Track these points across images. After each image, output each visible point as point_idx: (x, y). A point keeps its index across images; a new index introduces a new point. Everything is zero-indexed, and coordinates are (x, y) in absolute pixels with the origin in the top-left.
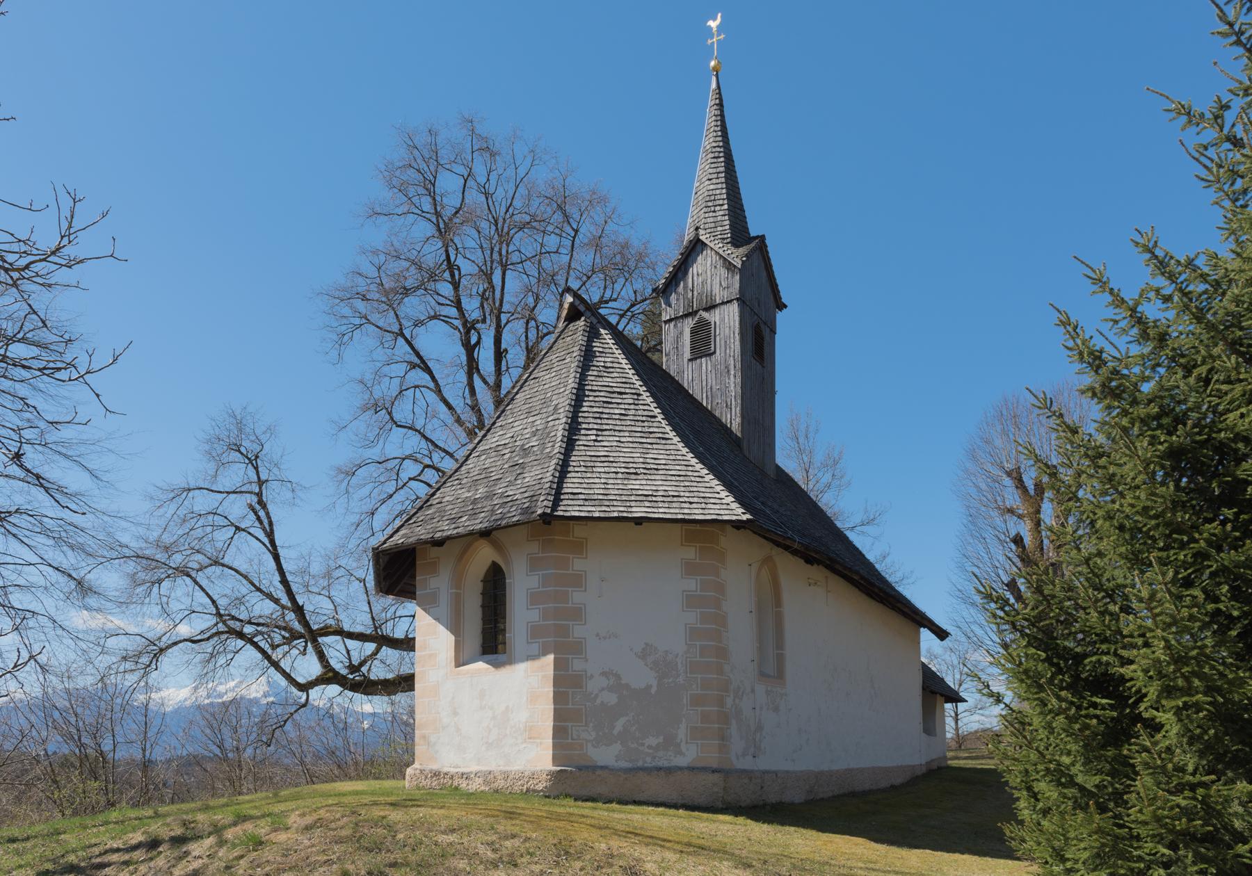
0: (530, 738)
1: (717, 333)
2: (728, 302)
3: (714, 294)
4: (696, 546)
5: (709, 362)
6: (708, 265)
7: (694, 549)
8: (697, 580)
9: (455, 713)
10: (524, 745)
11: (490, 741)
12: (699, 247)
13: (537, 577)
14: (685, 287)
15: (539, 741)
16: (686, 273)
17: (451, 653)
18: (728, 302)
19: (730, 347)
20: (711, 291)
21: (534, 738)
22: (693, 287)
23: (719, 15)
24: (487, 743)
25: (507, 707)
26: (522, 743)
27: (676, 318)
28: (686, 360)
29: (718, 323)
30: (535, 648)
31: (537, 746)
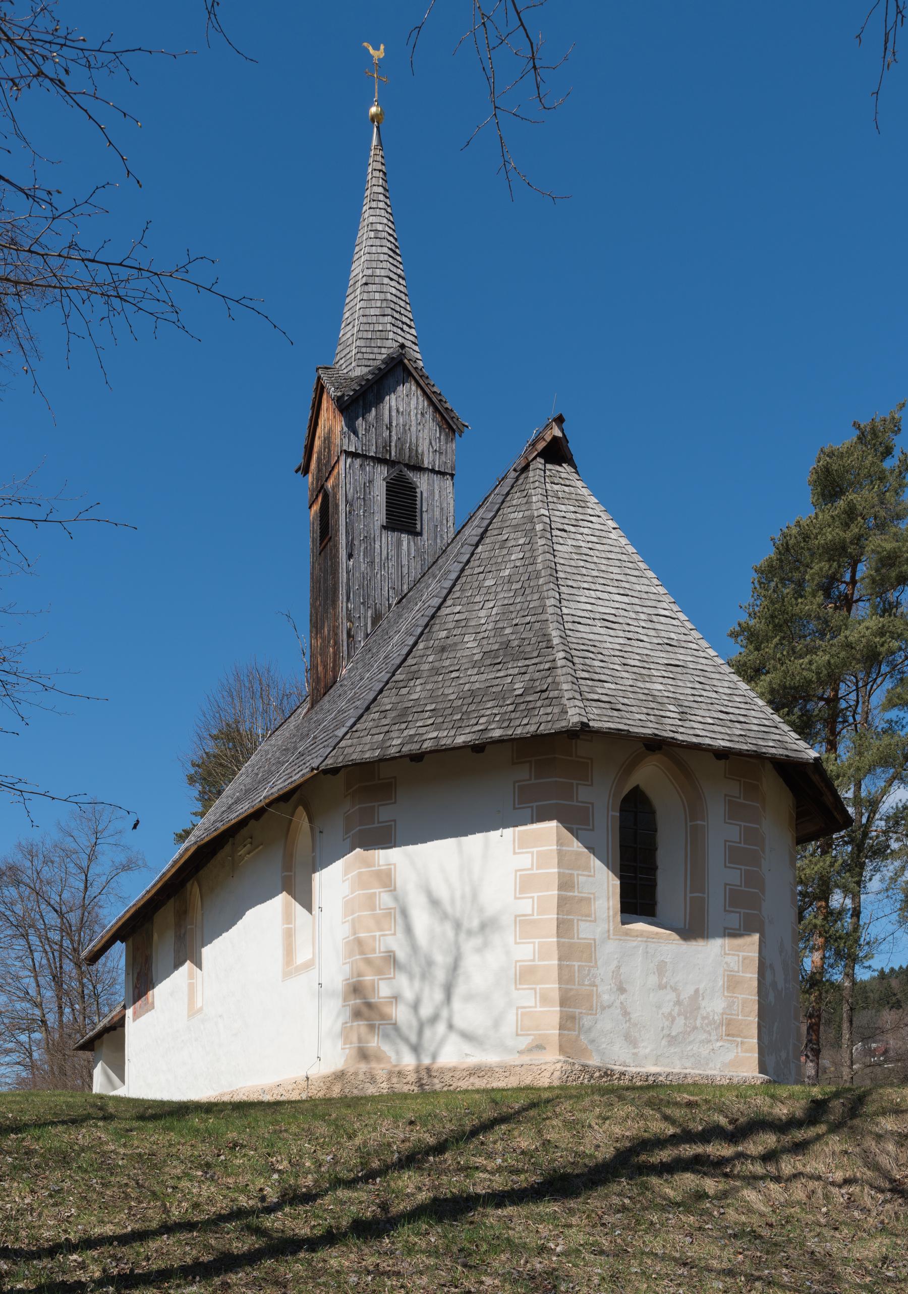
0: (728, 1035)
1: (424, 509)
2: (439, 473)
3: (420, 451)
4: (740, 826)
5: (412, 543)
6: (412, 406)
7: (529, 810)
8: (532, 853)
9: (622, 990)
10: (719, 1044)
11: (674, 1034)
12: (399, 370)
13: (529, 810)
14: (378, 418)
15: (739, 1039)
16: (379, 400)
17: (615, 902)
18: (439, 473)
19: (441, 536)
20: (417, 446)
21: (733, 1036)
22: (391, 423)
23: (365, 44)
24: (669, 1035)
25: (697, 991)
26: (717, 1040)
27: (365, 457)
28: (378, 525)
29: (425, 495)
30: (734, 920)
31: (737, 1046)
